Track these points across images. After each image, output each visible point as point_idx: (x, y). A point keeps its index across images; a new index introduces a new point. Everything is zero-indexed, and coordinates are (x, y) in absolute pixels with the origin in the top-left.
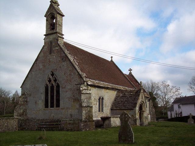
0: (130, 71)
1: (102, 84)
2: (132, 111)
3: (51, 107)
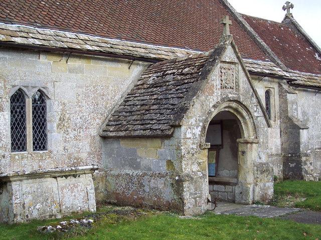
0: (288, 11)
1: (69, 38)
2: (166, 142)
3: (35, 149)
